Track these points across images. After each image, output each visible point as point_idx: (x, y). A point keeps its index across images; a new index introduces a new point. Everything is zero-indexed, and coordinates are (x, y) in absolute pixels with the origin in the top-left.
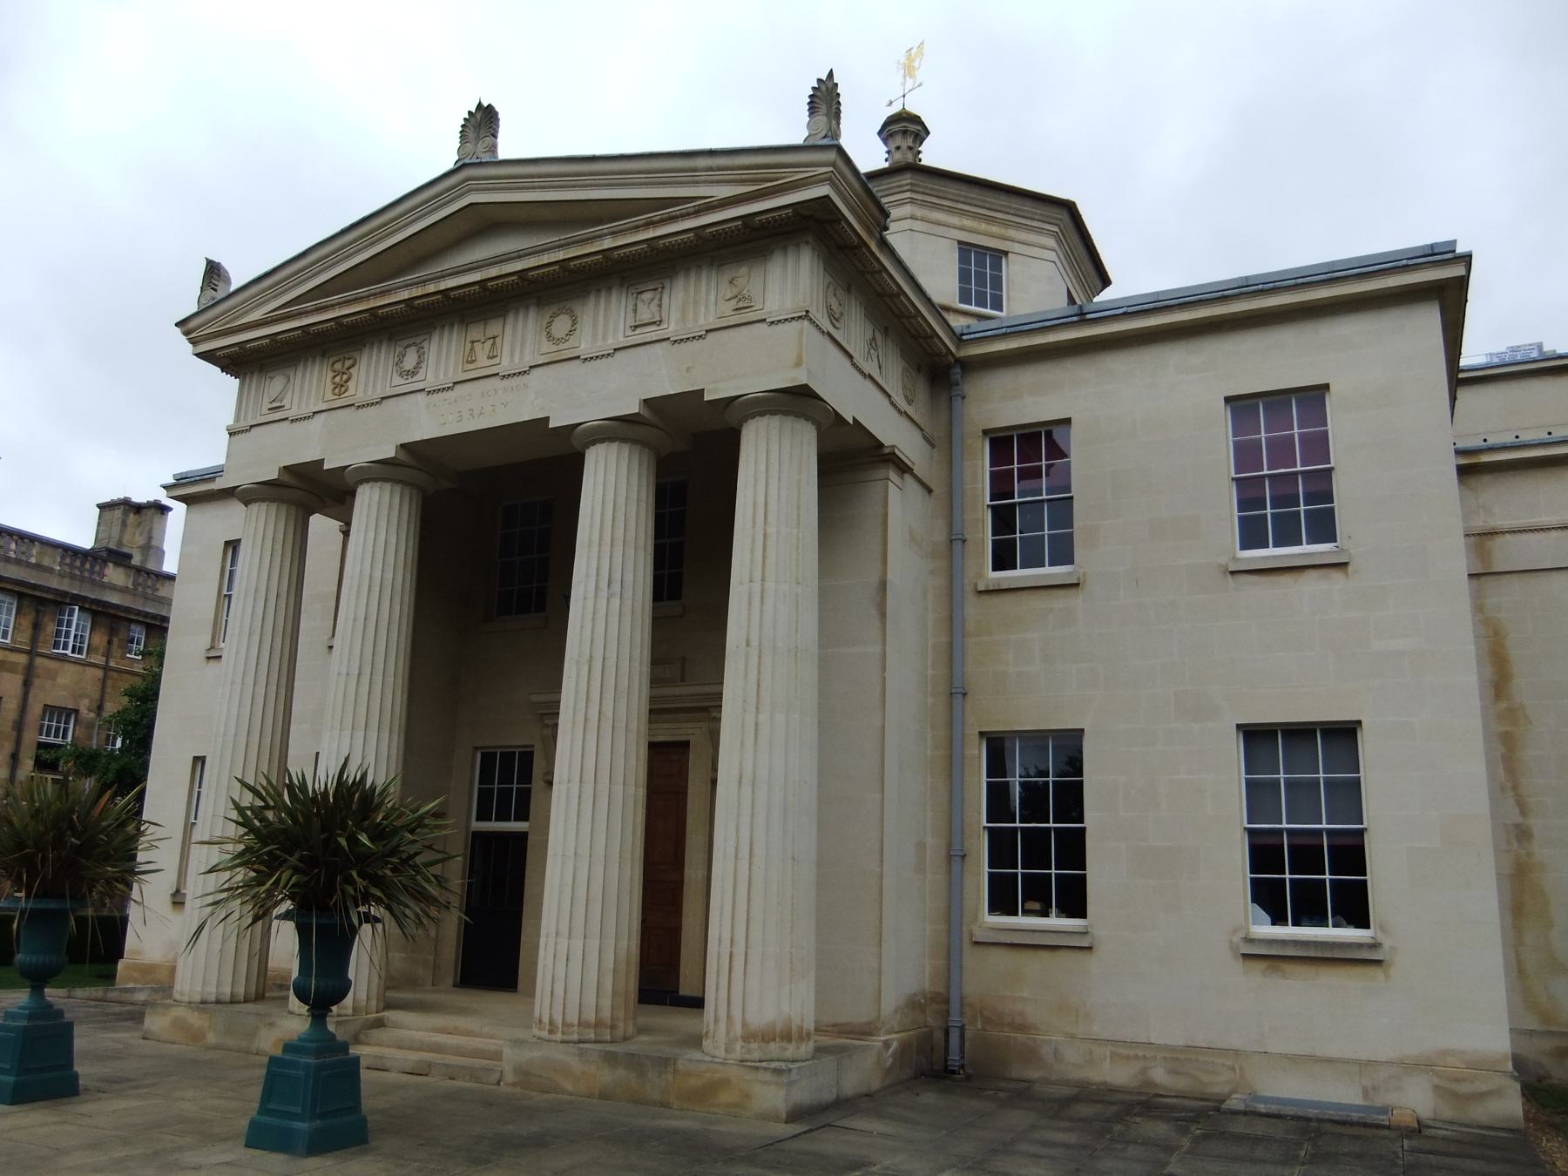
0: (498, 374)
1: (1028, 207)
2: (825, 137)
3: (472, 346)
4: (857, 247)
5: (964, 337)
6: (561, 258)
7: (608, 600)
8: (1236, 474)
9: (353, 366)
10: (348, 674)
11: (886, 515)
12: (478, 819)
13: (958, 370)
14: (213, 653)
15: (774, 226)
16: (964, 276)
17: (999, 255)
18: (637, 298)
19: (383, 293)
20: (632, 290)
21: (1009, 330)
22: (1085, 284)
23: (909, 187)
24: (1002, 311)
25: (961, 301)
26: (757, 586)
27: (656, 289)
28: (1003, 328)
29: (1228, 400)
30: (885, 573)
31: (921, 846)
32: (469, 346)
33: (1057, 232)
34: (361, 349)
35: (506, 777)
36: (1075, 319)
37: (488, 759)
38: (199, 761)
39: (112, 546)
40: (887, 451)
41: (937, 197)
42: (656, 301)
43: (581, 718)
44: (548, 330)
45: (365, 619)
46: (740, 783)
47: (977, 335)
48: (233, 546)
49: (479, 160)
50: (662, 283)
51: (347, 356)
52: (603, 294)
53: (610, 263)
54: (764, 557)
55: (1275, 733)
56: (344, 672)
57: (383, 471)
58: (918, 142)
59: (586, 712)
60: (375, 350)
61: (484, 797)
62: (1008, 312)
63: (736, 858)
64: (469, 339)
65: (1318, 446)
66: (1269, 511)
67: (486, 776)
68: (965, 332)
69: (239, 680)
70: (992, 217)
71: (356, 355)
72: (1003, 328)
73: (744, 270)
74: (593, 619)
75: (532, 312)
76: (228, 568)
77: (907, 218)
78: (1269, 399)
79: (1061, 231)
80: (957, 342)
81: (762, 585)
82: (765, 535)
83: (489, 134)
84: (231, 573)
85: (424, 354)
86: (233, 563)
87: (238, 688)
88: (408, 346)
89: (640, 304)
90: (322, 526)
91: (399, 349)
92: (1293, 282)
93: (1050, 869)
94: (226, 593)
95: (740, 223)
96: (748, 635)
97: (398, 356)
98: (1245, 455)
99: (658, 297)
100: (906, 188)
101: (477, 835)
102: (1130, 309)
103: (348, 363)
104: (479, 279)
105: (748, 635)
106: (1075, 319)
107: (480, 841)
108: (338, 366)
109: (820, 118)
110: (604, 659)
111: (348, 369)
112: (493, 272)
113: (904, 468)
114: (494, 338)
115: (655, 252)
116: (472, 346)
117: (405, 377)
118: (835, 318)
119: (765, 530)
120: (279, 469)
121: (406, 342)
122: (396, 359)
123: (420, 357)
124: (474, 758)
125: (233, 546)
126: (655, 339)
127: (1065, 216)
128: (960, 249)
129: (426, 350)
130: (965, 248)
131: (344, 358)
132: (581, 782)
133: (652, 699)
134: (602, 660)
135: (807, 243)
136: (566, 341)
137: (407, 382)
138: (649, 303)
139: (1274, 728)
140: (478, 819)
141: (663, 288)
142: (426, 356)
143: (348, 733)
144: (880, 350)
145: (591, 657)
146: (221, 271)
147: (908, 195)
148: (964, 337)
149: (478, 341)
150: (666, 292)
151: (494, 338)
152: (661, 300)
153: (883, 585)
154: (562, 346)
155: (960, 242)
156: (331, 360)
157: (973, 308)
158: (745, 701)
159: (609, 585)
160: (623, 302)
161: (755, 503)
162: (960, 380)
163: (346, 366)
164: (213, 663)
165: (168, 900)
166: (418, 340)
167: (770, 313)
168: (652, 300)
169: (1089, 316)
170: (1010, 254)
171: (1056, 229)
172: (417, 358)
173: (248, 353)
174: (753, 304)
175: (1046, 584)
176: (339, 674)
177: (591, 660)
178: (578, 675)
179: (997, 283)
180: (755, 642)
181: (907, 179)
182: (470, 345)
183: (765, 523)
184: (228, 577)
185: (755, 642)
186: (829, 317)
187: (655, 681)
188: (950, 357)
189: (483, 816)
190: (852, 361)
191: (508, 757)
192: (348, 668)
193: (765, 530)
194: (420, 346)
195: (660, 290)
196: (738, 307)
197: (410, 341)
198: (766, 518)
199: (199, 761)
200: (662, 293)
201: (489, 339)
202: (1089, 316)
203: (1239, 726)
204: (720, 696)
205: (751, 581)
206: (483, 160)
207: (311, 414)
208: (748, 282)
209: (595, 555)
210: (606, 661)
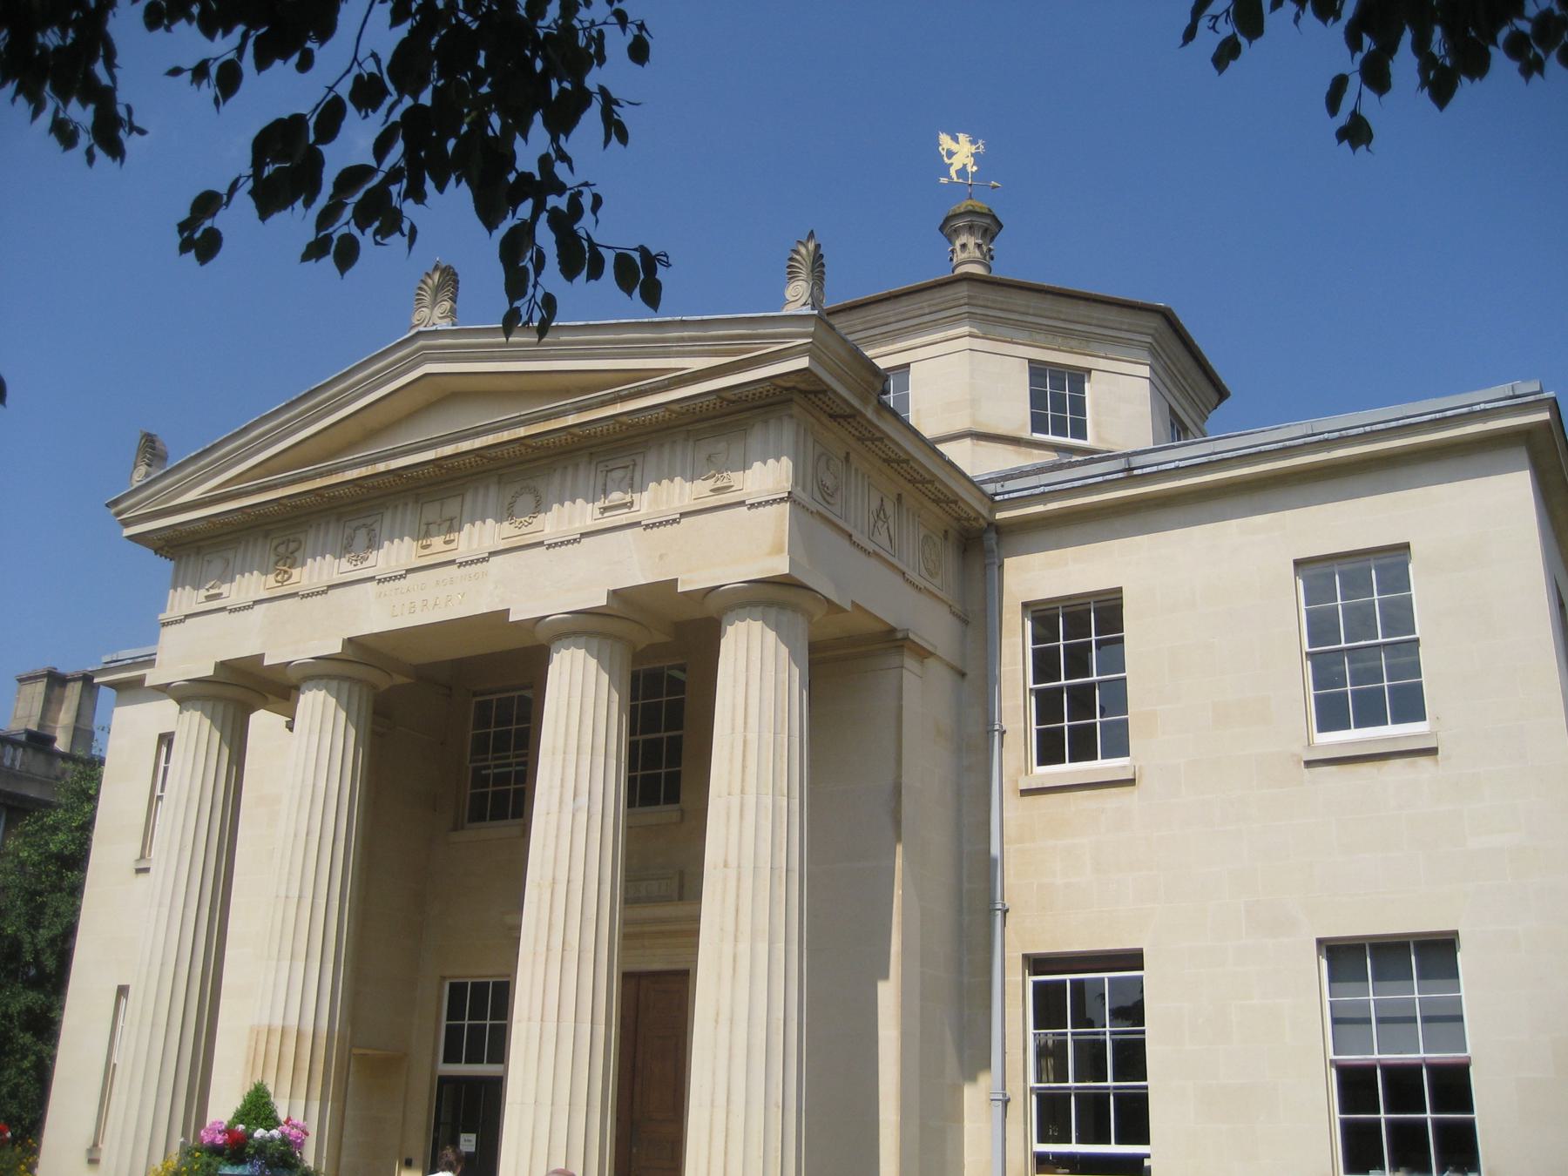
0: (454, 561)
1: (1112, 315)
2: (804, 304)
3: (428, 528)
4: (852, 416)
5: (997, 498)
6: (522, 435)
7: (574, 815)
8: (1310, 647)
9: (297, 550)
10: (287, 897)
11: (900, 707)
12: (446, 1060)
13: (993, 535)
14: (142, 865)
15: (760, 397)
16: (1037, 399)
17: (1079, 377)
18: (606, 476)
19: (330, 472)
20: (601, 467)
21: (1047, 489)
22: (1196, 399)
23: (966, 300)
24: (1085, 437)
25: (1034, 430)
26: (735, 800)
27: (627, 467)
28: (1041, 486)
29: (1298, 564)
30: (899, 776)
31: (102, 1143)
32: (423, 528)
33: (1151, 344)
34: (306, 531)
35: (478, 1013)
36: (1121, 475)
37: (457, 990)
38: (122, 991)
39: (33, 727)
40: (900, 635)
41: (1001, 309)
42: (627, 480)
43: (542, 949)
44: (510, 511)
45: (307, 834)
46: (717, 1022)
47: (1012, 495)
48: (166, 739)
49: (434, 328)
50: (634, 460)
51: (291, 537)
52: (570, 471)
53: (576, 439)
54: (744, 767)
55: (1406, 945)
56: (282, 894)
57: (322, 671)
58: (989, 238)
59: (548, 942)
60: (322, 534)
61: (453, 1034)
62: (1098, 437)
63: (712, 1105)
64: (424, 520)
65: (1400, 616)
66: (1349, 688)
67: (455, 1011)
68: (998, 491)
69: (167, 901)
70: (1072, 330)
71: (302, 536)
72: (1041, 486)
73: (722, 446)
74: (557, 836)
75: (493, 490)
76: (162, 764)
77: (965, 336)
78: (1347, 567)
79: (1156, 341)
80: (990, 503)
81: (742, 798)
82: (745, 742)
83: (446, 298)
84: (166, 770)
85: (375, 536)
86: (167, 760)
87: (165, 911)
88: (357, 528)
89: (609, 483)
90: (263, 723)
91: (348, 531)
92: (1361, 430)
93: (1424, 1112)
94: (159, 794)
95: (714, 397)
96: (726, 855)
97: (347, 539)
98: (1320, 628)
99: (629, 475)
100: (962, 302)
101: (444, 1081)
102: (1182, 464)
103: (292, 546)
104: (433, 457)
105: (726, 855)
106: (1121, 475)
107: (446, 1084)
108: (282, 549)
109: (800, 283)
110: (568, 881)
111: (292, 553)
112: (448, 450)
113: (923, 654)
114: (451, 520)
115: (624, 427)
116: (428, 528)
117: (354, 563)
118: (828, 494)
119: (745, 736)
120: (216, 665)
121: (355, 524)
122: (345, 542)
123: (370, 540)
124: (441, 987)
125: (166, 739)
126: (625, 523)
127: (1155, 322)
128: (1030, 368)
129: (377, 531)
130: (1037, 370)
131: (289, 540)
132: (542, 1020)
133: (625, 922)
134: (566, 882)
135: (791, 416)
136: (530, 524)
137: (355, 568)
138: (620, 482)
139: (1406, 940)
140: (446, 1060)
141: (635, 465)
142: (377, 539)
143: (286, 964)
144: (891, 521)
145: (554, 879)
146: (157, 444)
147: (965, 309)
148: (997, 498)
149: (435, 523)
150: (638, 469)
151: (451, 520)
152: (632, 479)
153: (897, 790)
154: (524, 530)
155: (1031, 361)
156: (275, 543)
157: (1050, 438)
158: (722, 929)
159: (574, 799)
160: (592, 477)
161: (734, 706)
162: (995, 547)
163: (290, 550)
164: (142, 876)
165: (82, 1158)
166: (369, 521)
167: (749, 494)
168: (624, 477)
169: (1136, 472)
170: (1093, 372)
171: (1149, 339)
172: (367, 541)
173: (184, 534)
174: (732, 484)
175: (172, 1081)
176: (277, 896)
177: (554, 883)
178: (540, 900)
179: (1079, 406)
180: (733, 862)
181: (963, 291)
182: (425, 527)
183: (745, 728)
184: (159, 775)
185: (733, 862)
186: (821, 492)
187: (629, 901)
188: (981, 520)
189: (451, 1056)
190: (851, 540)
191: (480, 988)
192: (287, 890)
193: (745, 736)
194: (372, 528)
195: (631, 467)
196: (715, 487)
197: (362, 522)
198: (745, 723)
199: (122, 991)
200: (633, 470)
201: (445, 521)
202: (1136, 472)
203: (1320, 942)
204: (697, 919)
205: (729, 794)
206: (439, 328)
207: (251, 603)
208: (727, 459)
209: (560, 764)
210: (571, 884)
